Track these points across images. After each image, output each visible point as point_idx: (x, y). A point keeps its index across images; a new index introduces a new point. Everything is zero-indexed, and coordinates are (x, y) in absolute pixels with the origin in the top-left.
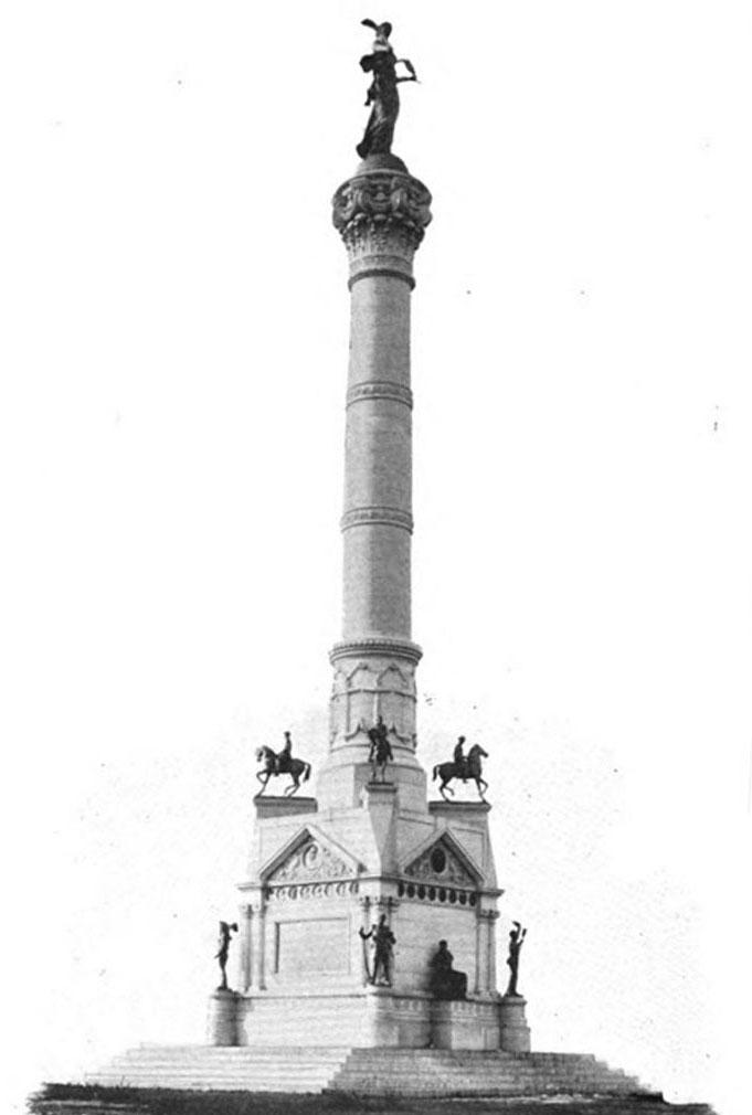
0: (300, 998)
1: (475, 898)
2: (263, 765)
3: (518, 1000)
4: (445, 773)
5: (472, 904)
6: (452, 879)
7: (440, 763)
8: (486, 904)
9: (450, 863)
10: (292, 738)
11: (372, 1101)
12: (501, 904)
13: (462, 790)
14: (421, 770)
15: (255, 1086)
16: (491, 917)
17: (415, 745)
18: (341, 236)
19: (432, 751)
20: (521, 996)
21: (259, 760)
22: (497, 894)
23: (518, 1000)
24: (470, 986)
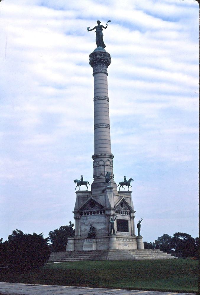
0: (105, 238)
1: (130, 213)
2: (76, 184)
3: (140, 237)
4: (122, 184)
5: (129, 215)
6: (125, 209)
7: (121, 182)
8: (132, 214)
9: (124, 205)
10: (83, 177)
11: (88, 285)
12: (135, 214)
13: (126, 188)
14: (115, 183)
15: (198, 197)
16: (134, 217)
17: (113, 178)
18: (93, 73)
19: (118, 179)
20: (141, 236)
21: (75, 183)
22: (135, 212)
23: (140, 237)
24: (76, 234)
